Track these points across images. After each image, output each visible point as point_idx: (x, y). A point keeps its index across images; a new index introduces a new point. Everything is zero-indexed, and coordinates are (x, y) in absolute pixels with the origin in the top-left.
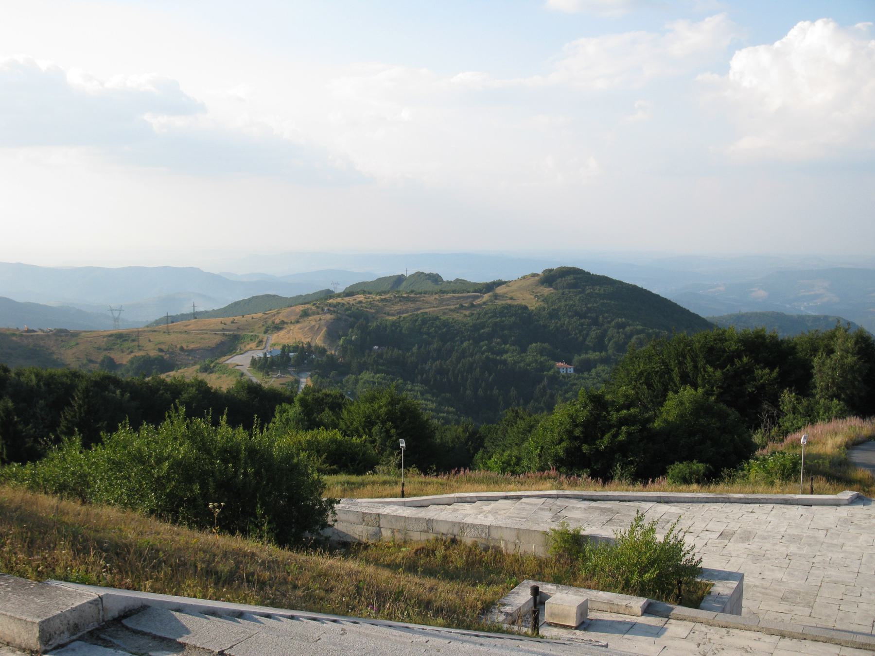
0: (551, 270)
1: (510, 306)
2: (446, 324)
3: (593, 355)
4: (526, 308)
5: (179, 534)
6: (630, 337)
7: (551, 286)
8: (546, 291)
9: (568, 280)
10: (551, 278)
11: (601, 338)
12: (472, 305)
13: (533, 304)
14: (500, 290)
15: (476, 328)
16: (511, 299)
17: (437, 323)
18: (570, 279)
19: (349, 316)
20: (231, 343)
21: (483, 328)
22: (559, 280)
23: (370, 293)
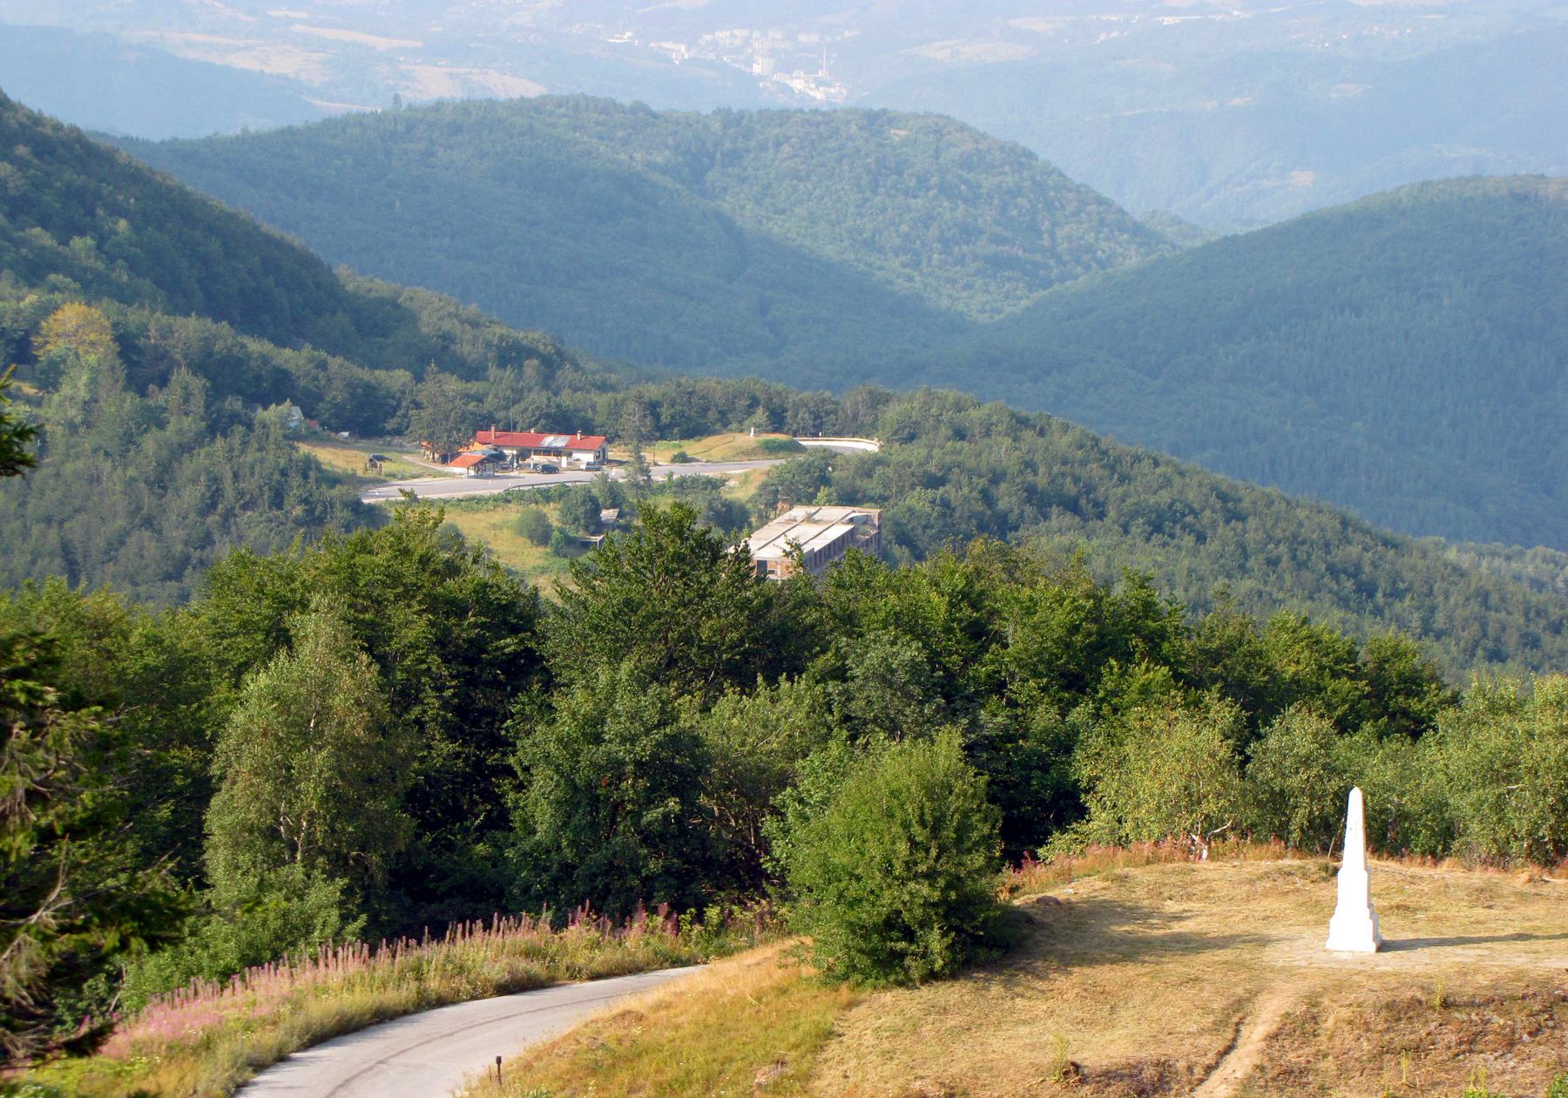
20: (517, 388)
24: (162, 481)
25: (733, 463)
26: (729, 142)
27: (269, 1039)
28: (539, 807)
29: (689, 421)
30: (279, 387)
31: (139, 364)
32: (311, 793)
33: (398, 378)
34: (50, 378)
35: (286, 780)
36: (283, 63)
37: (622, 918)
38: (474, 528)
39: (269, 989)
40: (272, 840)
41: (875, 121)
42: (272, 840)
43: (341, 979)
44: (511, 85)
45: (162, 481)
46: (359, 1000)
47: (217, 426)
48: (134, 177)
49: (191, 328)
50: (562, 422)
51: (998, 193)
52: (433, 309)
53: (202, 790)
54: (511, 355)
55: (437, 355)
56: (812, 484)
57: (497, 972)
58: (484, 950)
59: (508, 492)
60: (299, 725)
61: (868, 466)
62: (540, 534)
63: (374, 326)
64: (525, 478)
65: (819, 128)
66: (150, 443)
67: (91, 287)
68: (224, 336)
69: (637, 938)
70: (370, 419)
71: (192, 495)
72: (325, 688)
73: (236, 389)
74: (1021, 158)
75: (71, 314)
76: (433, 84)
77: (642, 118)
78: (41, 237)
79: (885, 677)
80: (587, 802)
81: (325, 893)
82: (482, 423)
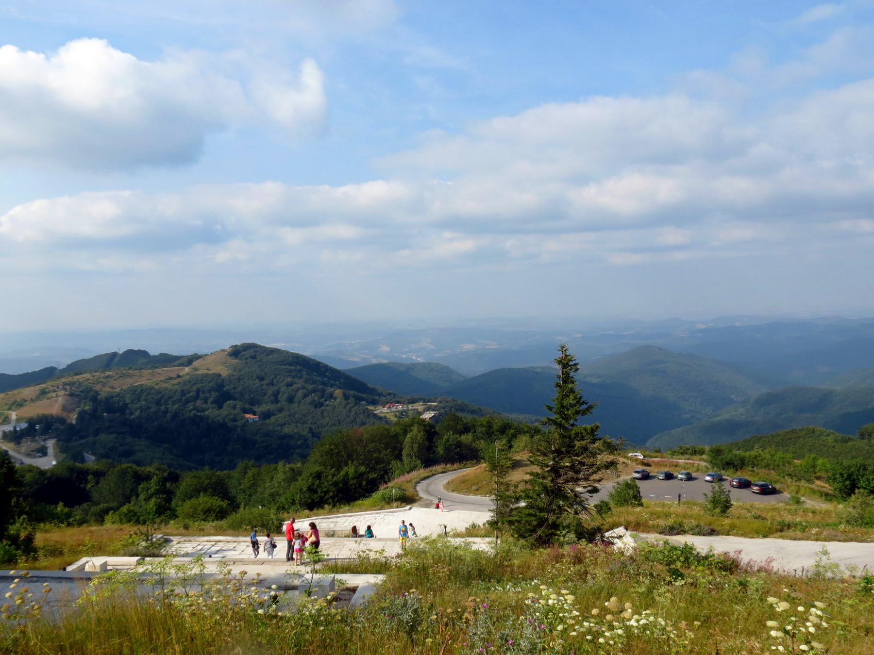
0: (236, 346)
1: (207, 375)
2: (158, 392)
3: (271, 407)
4: (220, 375)
5: (676, 466)
6: (297, 390)
7: (237, 358)
8: (235, 361)
9: (161, 354)
10: (236, 352)
11: (276, 394)
12: (179, 376)
13: (225, 372)
14: (196, 364)
15: (183, 393)
16: (208, 369)
17: (153, 391)
18: (251, 352)
19: (82, 392)
20: (393, 398)
21: (189, 393)
22: (243, 353)
23: (96, 372)
24: (350, 411)
25: (419, 406)
26: (413, 366)
27: (417, 480)
28: (440, 450)
29: (413, 402)
30: (363, 399)
31: (346, 397)
32: (415, 449)
33: (377, 398)
34: (335, 399)
35: (412, 447)
36: (356, 359)
37: (453, 464)
38: (388, 416)
39: (414, 474)
40: (410, 455)
41: (430, 364)
42: (410, 455)
43: (423, 472)
44: (384, 361)
45: (350, 411)
46: (426, 475)
47: (356, 404)
48: (343, 374)
49: (352, 392)
50: (398, 402)
51: (445, 372)
52: (380, 389)
53: (401, 450)
54: (390, 394)
55: (380, 395)
56: (429, 409)
57: (440, 470)
58: (439, 468)
59: (32, 423)
60: (413, 441)
61: (436, 406)
62: (396, 416)
63: (373, 391)
64: (393, 409)
65: (423, 364)
66: (348, 406)
67: (340, 388)
68: (356, 393)
69: (455, 466)
70: (374, 403)
71: (353, 413)
72: (416, 436)
73: (358, 399)
74: (448, 368)
75: (338, 391)
76: (374, 361)
77: (401, 365)
78: (332, 382)
79: (481, 432)
80: (447, 449)
81: (418, 462)
82: (388, 403)
